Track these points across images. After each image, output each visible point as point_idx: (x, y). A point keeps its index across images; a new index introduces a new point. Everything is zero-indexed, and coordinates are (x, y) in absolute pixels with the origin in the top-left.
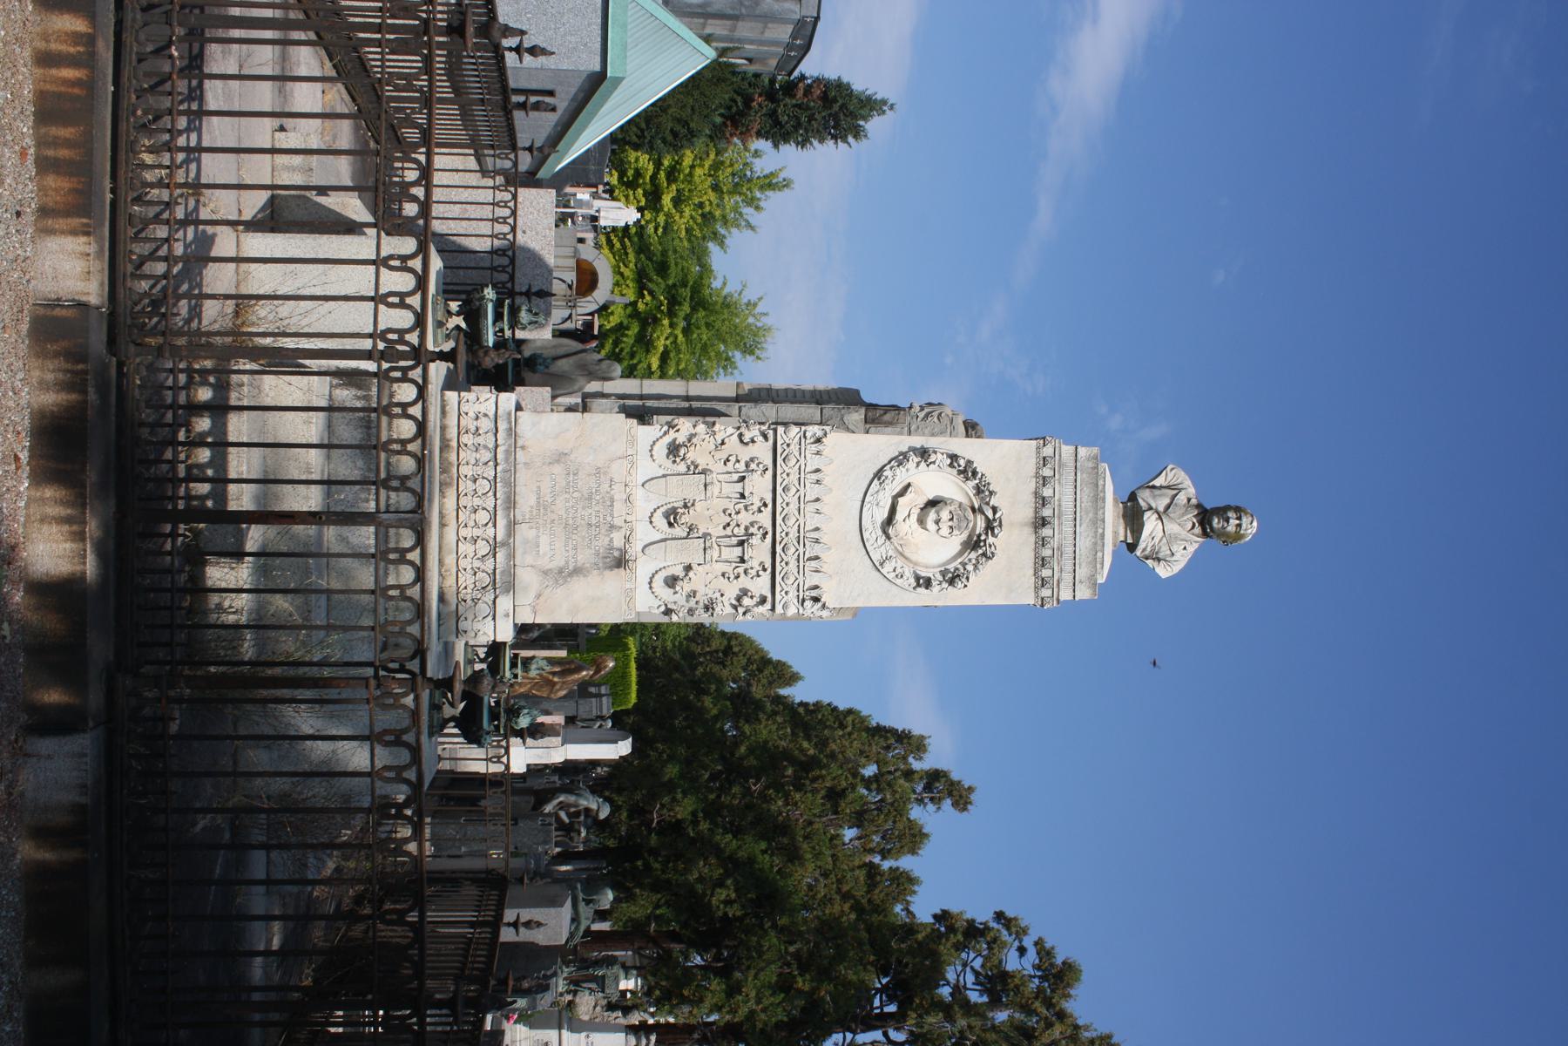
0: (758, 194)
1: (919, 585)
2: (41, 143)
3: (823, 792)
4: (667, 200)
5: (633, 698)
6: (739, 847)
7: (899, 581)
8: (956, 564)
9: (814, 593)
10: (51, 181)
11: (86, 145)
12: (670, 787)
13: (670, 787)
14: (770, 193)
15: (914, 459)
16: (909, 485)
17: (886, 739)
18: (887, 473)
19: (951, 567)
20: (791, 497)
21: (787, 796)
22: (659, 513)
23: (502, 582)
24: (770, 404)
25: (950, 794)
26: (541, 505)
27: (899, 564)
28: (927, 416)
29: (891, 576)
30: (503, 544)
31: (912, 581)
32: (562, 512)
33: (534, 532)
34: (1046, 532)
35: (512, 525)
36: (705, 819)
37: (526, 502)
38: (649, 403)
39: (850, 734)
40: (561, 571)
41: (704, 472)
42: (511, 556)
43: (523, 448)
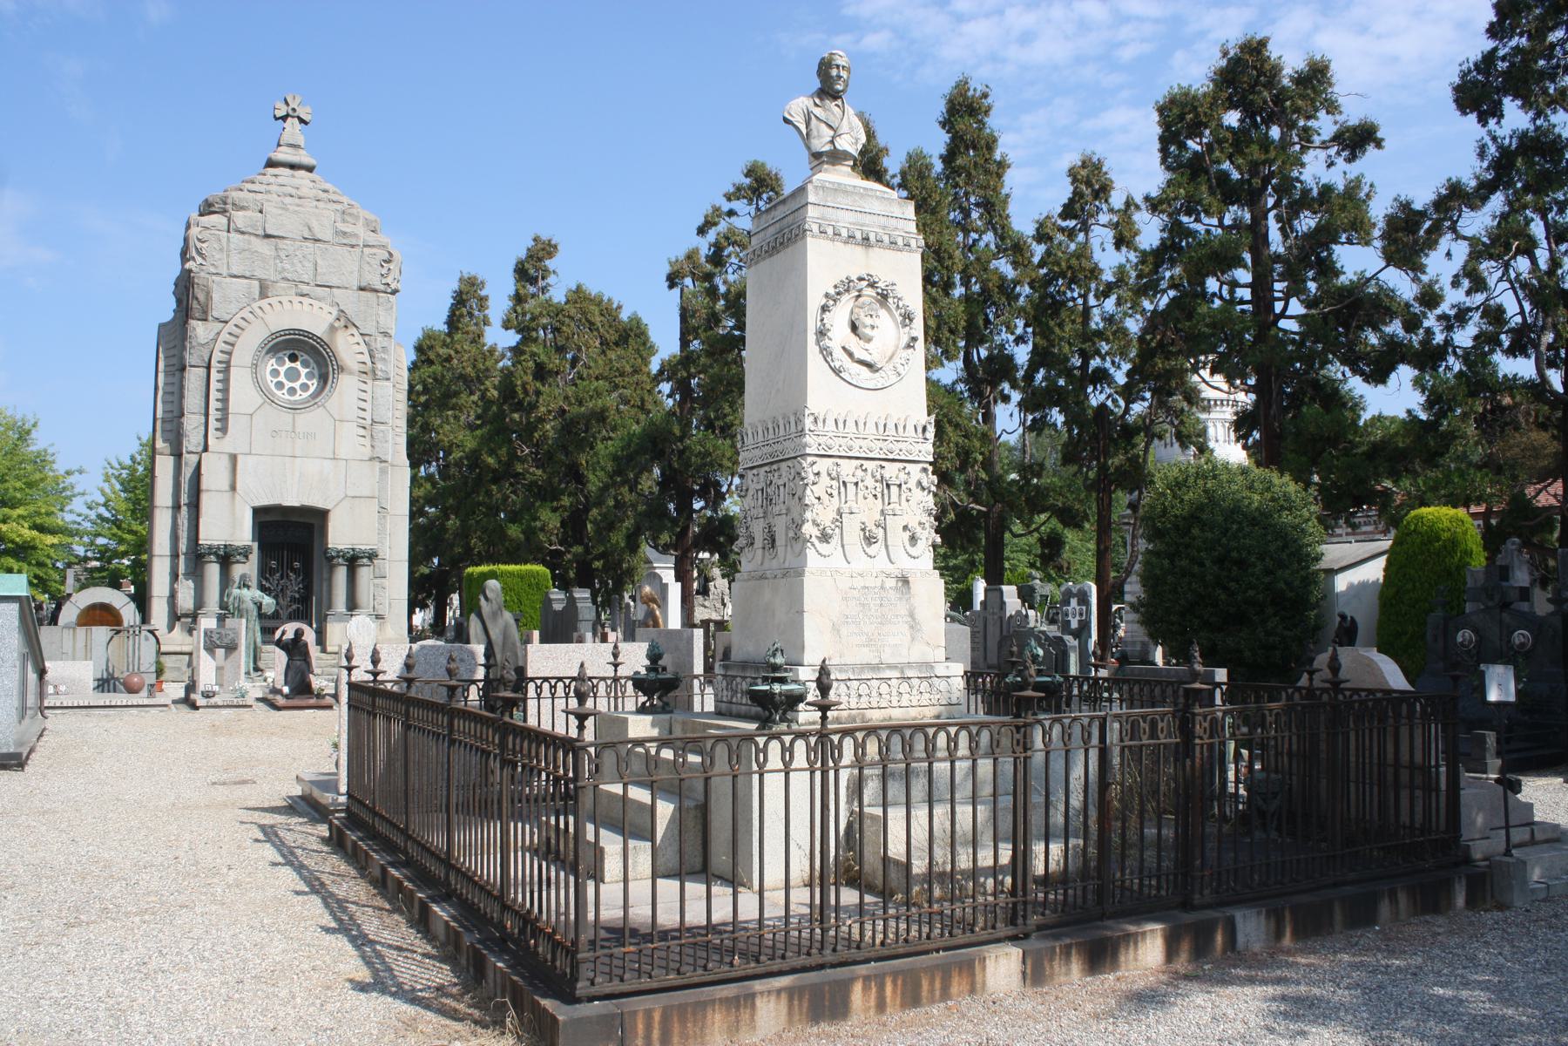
2: (932, 1001)
5: (539, 568)
8: (897, 314)
9: (920, 430)
10: (954, 990)
11: (931, 970)
12: (530, 533)
13: (530, 533)
15: (826, 342)
17: (462, 316)
20: (896, 447)
21: (541, 420)
23: (927, 673)
24: (185, 420)
25: (540, 260)
28: (200, 254)
34: (872, 237)
35: (891, 667)
36: (559, 500)
37: (868, 656)
38: (183, 547)
39: (457, 352)
41: (840, 514)
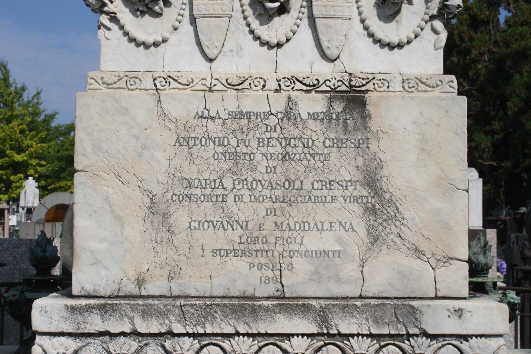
0: (13, 89)
3: (472, 33)
4: (19, 158)
6: (517, 96)
14: (11, 80)
21: (475, 61)
22: (263, 31)
26: (250, 246)
30: (323, 318)
32: (261, 208)
33: (298, 262)
37: (241, 276)
40: (371, 211)
42: (346, 304)
43: (140, 282)
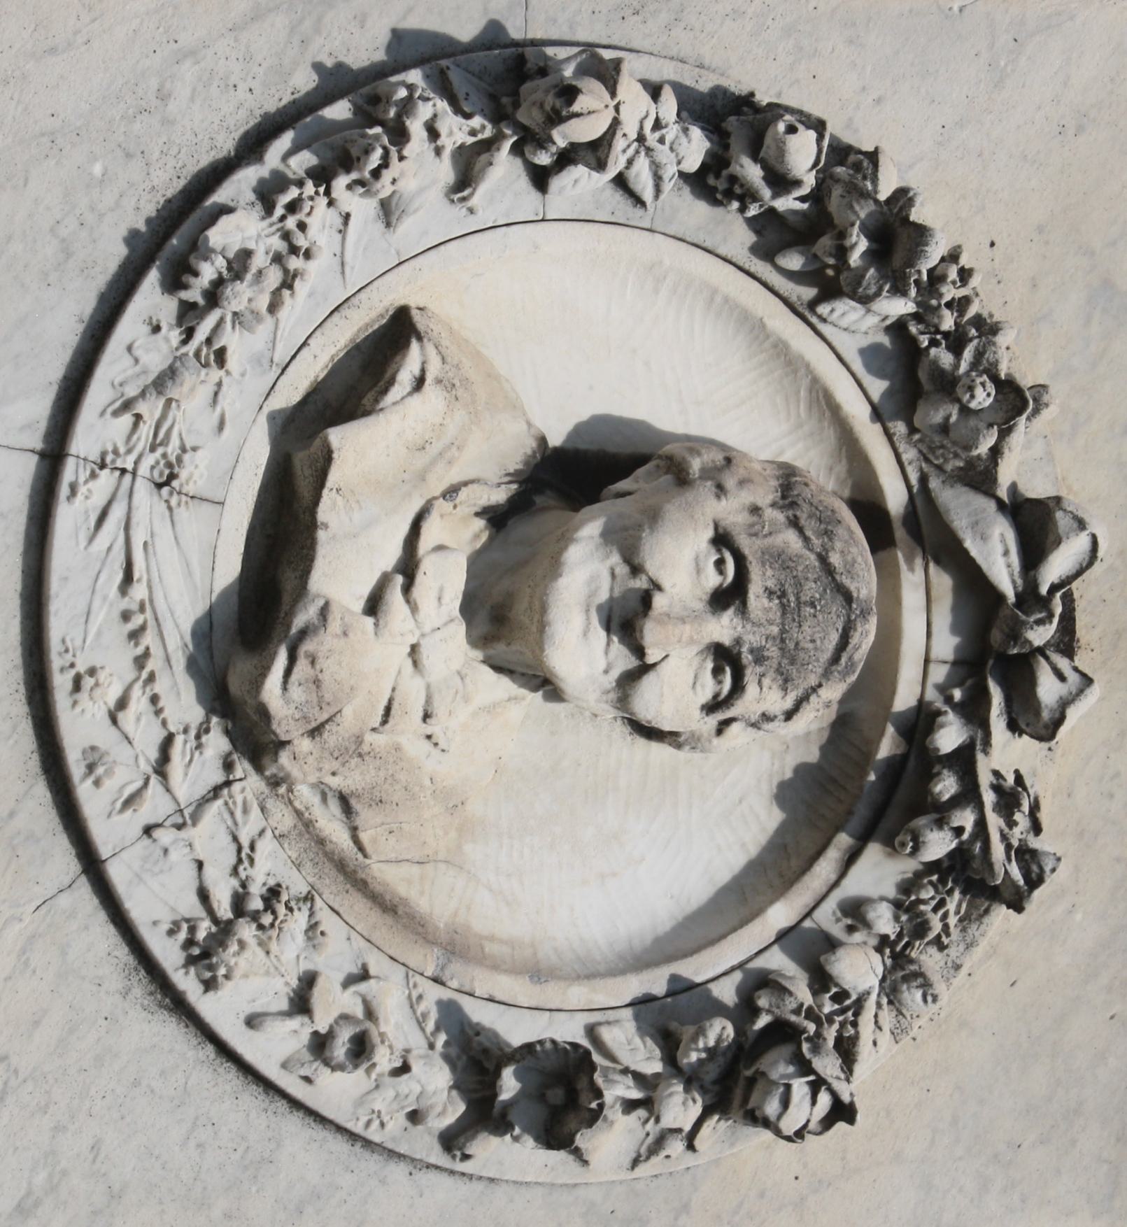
1: (484, 1114)
7: (336, 1090)
8: (754, 941)
16: (399, 330)
18: (240, 229)
19: (716, 967)
27: (333, 962)
29: (272, 1049)
31: (435, 1081)
